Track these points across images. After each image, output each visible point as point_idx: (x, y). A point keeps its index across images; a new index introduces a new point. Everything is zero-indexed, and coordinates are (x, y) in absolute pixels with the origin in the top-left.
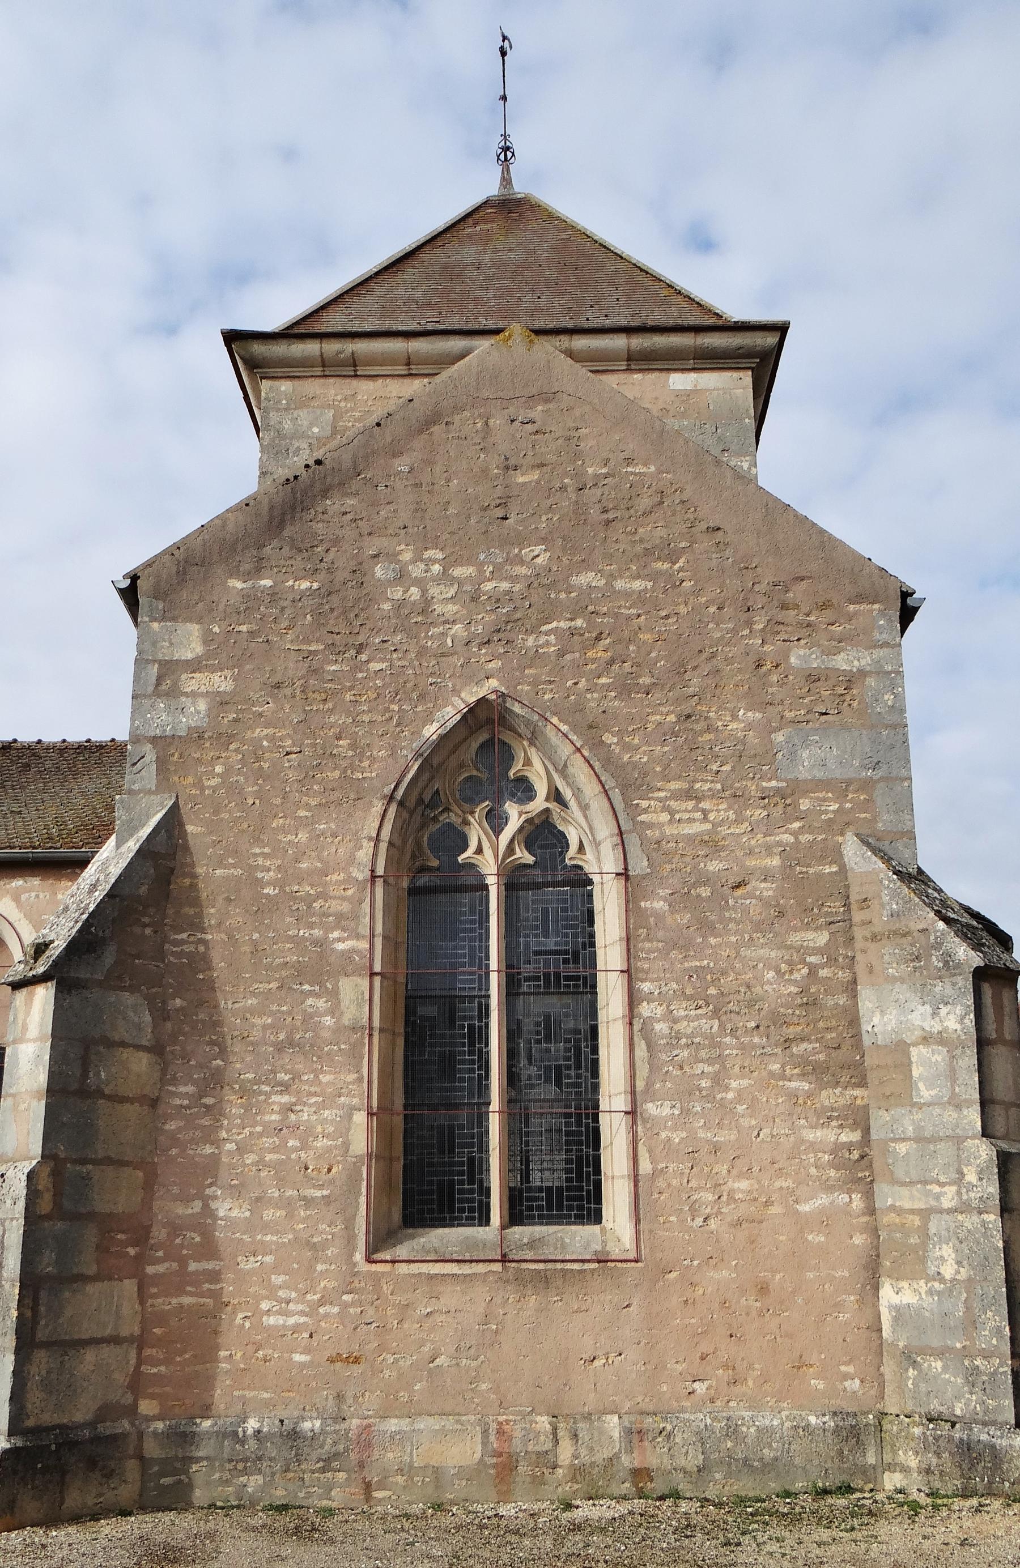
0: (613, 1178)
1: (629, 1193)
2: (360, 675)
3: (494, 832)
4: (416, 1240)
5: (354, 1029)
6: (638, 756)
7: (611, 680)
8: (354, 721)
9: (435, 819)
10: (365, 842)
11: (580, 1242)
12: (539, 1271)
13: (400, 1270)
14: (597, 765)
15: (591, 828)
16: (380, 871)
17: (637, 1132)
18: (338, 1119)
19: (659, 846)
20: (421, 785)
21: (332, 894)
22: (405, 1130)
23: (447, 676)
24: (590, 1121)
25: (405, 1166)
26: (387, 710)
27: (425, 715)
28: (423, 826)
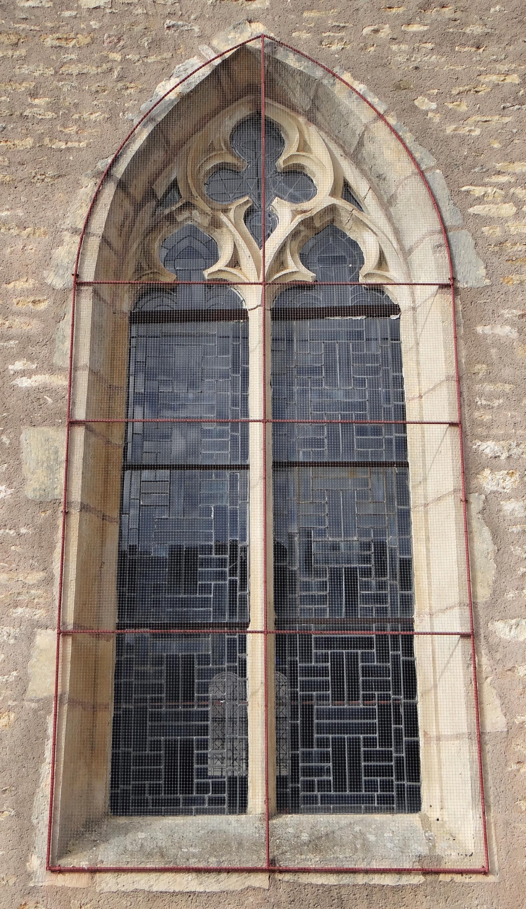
0: (438, 739)
1: (472, 762)
2: (67, 14)
3: (256, 239)
4: (130, 835)
5: (41, 504)
6: (467, 129)
7: (426, 28)
8: (56, 72)
9: (171, 218)
10: (67, 236)
11: (392, 841)
12: (328, 889)
13: (103, 885)
14: (408, 138)
15: (397, 232)
16: (88, 275)
17: (480, 665)
18: (12, 641)
19: (501, 249)
20: (151, 167)
21: (15, 308)
22: (118, 664)
23: (193, 17)
24: (400, 652)
25: (116, 720)
26: (105, 59)
27: (160, 67)
28: (153, 229)
